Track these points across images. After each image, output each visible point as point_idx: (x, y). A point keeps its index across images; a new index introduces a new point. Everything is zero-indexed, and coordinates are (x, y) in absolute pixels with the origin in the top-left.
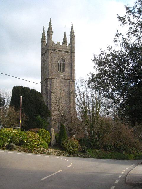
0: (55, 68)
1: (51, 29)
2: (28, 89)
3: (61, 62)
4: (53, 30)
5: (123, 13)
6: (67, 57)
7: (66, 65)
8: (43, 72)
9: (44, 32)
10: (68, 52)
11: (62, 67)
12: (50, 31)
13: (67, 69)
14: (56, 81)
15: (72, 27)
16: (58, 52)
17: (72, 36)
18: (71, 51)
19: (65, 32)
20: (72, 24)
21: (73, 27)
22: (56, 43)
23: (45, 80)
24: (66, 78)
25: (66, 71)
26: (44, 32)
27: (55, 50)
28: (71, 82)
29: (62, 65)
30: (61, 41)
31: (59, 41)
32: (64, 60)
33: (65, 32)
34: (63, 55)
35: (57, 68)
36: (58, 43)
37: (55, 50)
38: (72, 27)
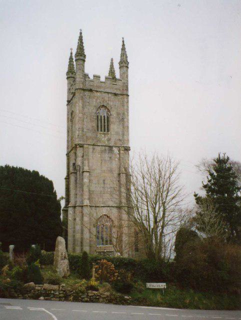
1: (113, 66)
4: (86, 52)
6: (113, 102)
8: (70, 134)
9: (71, 53)
10: (115, 94)
11: (103, 125)
12: (81, 54)
13: (114, 127)
14: (94, 149)
15: (123, 45)
17: (124, 64)
18: (122, 94)
20: (123, 41)
21: (126, 46)
22: (91, 77)
23: (74, 172)
24: (112, 144)
26: (71, 58)
27: (91, 90)
28: (122, 152)
29: (104, 119)
30: (104, 74)
31: (97, 74)
32: (108, 110)
33: (112, 60)
34: (106, 99)
35: (95, 125)
36: (97, 77)
38: (123, 45)
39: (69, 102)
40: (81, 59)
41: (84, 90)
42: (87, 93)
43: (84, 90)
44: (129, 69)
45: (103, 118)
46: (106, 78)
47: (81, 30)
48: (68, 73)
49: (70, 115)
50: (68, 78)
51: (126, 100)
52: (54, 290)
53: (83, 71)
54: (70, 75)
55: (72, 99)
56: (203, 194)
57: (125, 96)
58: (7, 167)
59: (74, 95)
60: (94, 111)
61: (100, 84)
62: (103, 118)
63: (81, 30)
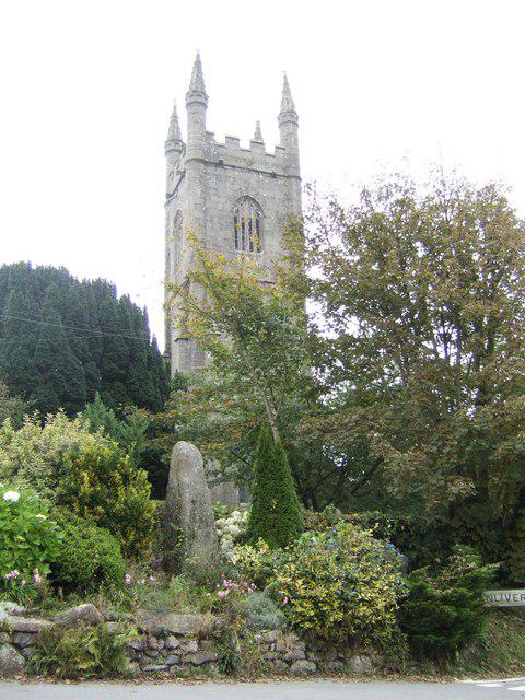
0: (222, 234)
2: (474, 674)
3: (248, 212)
5: (373, 188)
6: (270, 193)
7: (267, 227)
9: (175, 118)
10: (274, 176)
12: (197, 99)
15: (286, 84)
16: (230, 173)
17: (289, 118)
19: (258, 123)
21: (291, 86)
25: (267, 248)
26: (175, 118)
27: (220, 164)
29: (250, 229)
33: (258, 123)
34: (253, 183)
35: (230, 234)
36: (232, 140)
37: (220, 164)
38: (286, 84)
39: (169, 196)
40: (199, 102)
41: (206, 163)
42: (211, 169)
43: (206, 163)
44: (299, 129)
45: (247, 224)
46: (252, 142)
47: (198, 51)
48: (168, 143)
49: (172, 224)
50: (168, 152)
51: (295, 188)
52: (178, 636)
53: (203, 125)
54: (173, 146)
55: (176, 190)
56: (34, 267)
57: (293, 180)
58: (22, 270)
59: (183, 176)
60: (229, 206)
61: (239, 154)
62: (247, 224)
63: (175, 100)
